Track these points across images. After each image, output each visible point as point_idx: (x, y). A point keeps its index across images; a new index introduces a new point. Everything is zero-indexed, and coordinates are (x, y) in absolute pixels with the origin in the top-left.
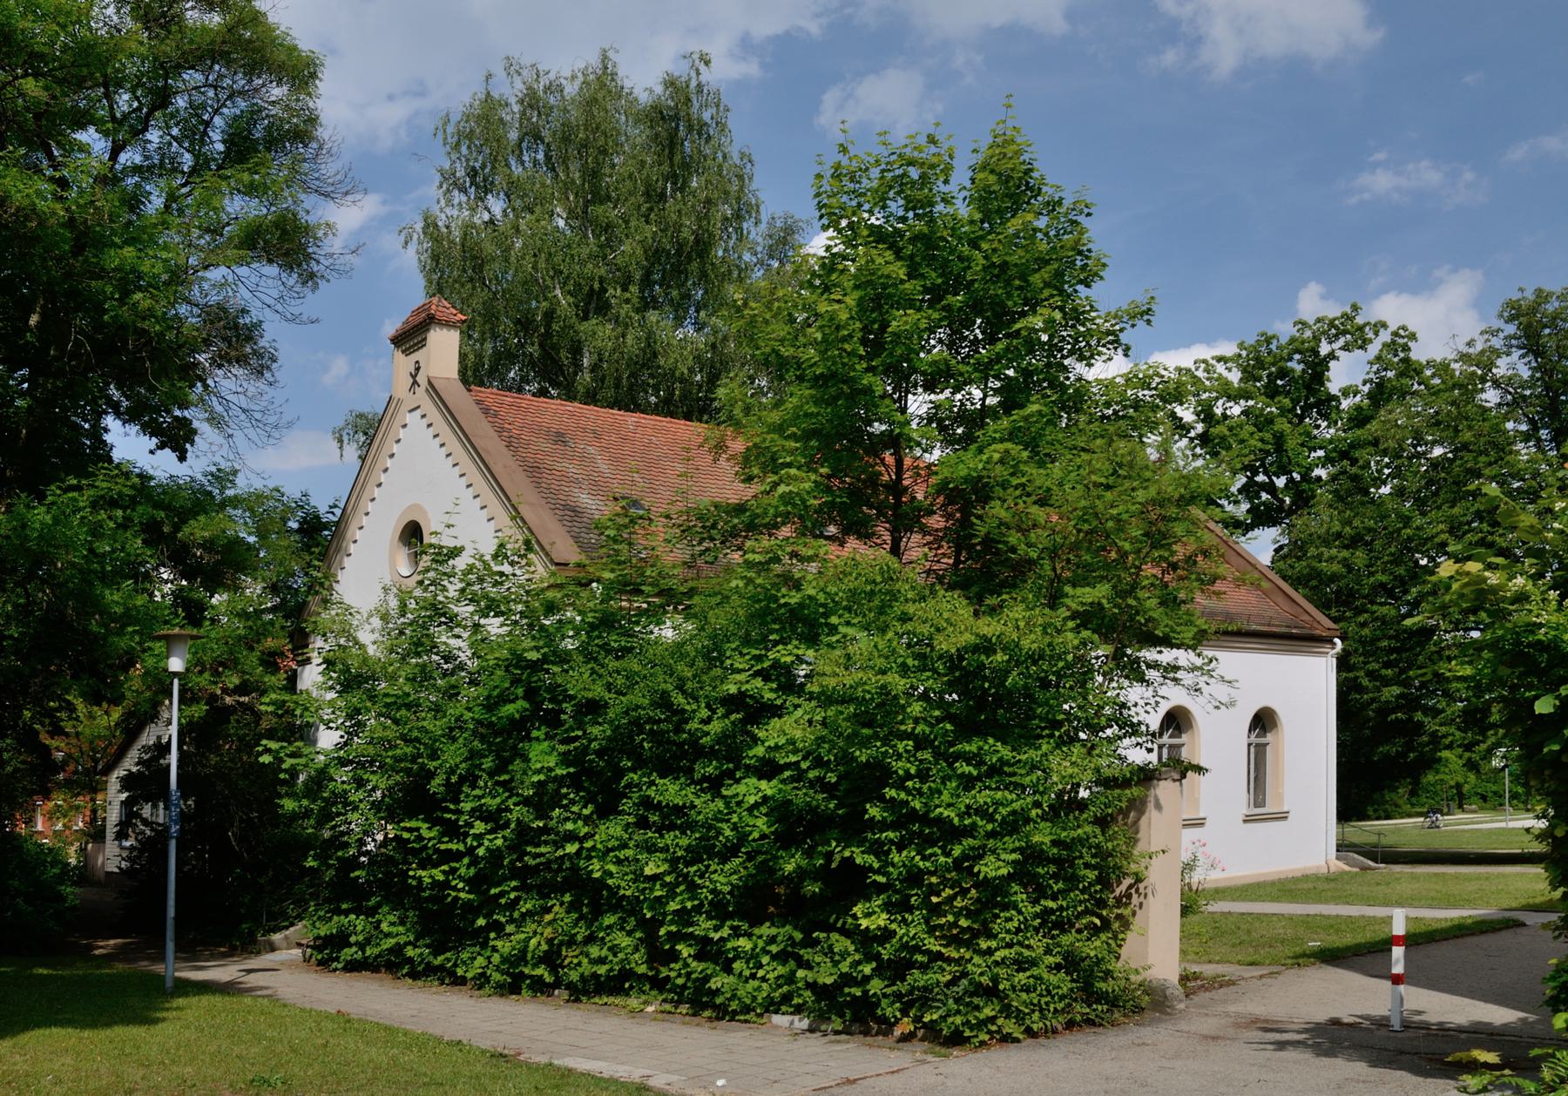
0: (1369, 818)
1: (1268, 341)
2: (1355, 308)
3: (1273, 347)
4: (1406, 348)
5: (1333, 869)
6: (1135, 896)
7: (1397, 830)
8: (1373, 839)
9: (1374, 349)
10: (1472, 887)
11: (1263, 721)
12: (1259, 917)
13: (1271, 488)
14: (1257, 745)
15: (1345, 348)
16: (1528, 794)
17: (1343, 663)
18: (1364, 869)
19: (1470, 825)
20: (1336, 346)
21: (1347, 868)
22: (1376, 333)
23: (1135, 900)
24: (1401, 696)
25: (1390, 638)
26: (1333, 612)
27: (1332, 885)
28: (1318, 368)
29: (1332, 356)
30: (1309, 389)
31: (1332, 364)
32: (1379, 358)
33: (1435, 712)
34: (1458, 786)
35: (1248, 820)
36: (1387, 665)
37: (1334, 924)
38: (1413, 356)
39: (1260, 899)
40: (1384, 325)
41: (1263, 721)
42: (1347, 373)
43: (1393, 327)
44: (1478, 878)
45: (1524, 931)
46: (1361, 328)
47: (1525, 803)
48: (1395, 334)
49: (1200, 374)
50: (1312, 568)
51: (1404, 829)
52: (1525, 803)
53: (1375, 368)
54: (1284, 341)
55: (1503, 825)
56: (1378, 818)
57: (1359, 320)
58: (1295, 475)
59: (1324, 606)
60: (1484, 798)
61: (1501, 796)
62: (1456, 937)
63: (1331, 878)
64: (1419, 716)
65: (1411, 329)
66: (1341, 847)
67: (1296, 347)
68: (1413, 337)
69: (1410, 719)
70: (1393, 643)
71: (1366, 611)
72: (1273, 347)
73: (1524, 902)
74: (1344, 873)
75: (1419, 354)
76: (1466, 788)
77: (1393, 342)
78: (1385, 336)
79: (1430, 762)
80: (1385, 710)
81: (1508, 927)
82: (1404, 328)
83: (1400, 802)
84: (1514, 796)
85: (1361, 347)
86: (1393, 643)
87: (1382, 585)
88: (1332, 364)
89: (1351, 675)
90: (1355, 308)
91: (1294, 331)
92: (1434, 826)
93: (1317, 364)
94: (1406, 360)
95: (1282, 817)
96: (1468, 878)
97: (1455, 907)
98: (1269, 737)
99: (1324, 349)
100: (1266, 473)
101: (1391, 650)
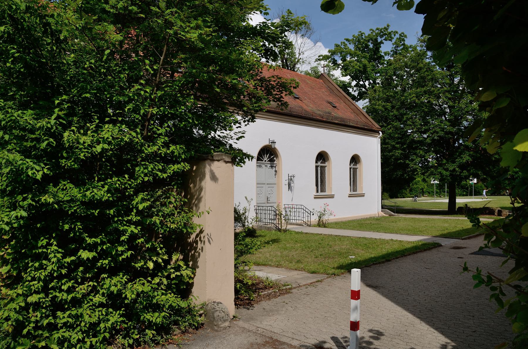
0: (398, 198)
1: (362, 34)
2: (388, 26)
3: (363, 37)
4: (404, 40)
5: (380, 215)
6: (199, 242)
7: (406, 201)
8: (393, 204)
9: (394, 41)
10: (423, 224)
11: (355, 160)
12: (340, 238)
13: (364, 86)
14: (353, 168)
15: (386, 40)
16: (440, 192)
17: (383, 142)
18: (390, 215)
19: (425, 201)
20: (383, 39)
21: (384, 215)
22: (395, 35)
23: (200, 245)
24: (401, 154)
25: (398, 134)
26: (381, 124)
27: (378, 222)
28: (377, 45)
29: (381, 42)
30: (375, 56)
31: (382, 45)
32: (395, 43)
33: (413, 160)
34: (422, 189)
35: (350, 196)
36: (397, 143)
37: (369, 243)
38: (406, 43)
39: (341, 228)
40: (397, 32)
41: (355, 160)
42: (386, 47)
43: (400, 33)
44: (426, 220)
45: (440, 249)
46: (390, 33)
47: (440, 195)
48: (400, 35)
49: (342, 47)
50: (374, 108)
51: (406, 202)
52: (440, 195)
53: (394, 46)
54: (367, 35)
55: (434, 201)
56: (401, 198)
57: (389, 31)
58: (371, 81)
59: (378, 122)
60: (429, 193)
61: (434, 193)
62: (414, 253)
63: (378, 219)
64: (407, 162)
65: (405, 34)
66: (383, 207)
67: (370, 39)
68: (406, 36)
69: (405, 162)
70: (399, 136)
71: (391, 124)
72: (363, 37)
73: (441, 233)
74: (383, 217)
75: (408, 42)
76: (424, 190)
77: (400, 38)
78: (397, 36)
79: (412, 179)
80: (397, 159)
81: (435, 247)
82: (403, 33)
83: (407, 193)
84: (437, 193)
85: (390, 40)
86: (399, 136)
87: (396, 116)
88: (382, 45)
89: (386, 146)
90: (388, 26)
91: (370, 33)
92: (415, 201)
93: (377, 45)
94: (404, 44)
95: (362, 195)
96: (423, 220)
97: (416, 235)
98: (358, 166)
99: (379, 40)
100: (363, 81)
101: (398, 138)
